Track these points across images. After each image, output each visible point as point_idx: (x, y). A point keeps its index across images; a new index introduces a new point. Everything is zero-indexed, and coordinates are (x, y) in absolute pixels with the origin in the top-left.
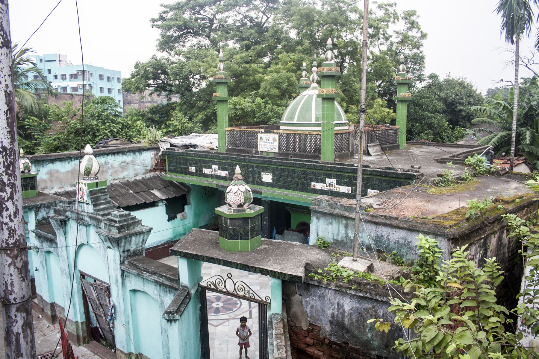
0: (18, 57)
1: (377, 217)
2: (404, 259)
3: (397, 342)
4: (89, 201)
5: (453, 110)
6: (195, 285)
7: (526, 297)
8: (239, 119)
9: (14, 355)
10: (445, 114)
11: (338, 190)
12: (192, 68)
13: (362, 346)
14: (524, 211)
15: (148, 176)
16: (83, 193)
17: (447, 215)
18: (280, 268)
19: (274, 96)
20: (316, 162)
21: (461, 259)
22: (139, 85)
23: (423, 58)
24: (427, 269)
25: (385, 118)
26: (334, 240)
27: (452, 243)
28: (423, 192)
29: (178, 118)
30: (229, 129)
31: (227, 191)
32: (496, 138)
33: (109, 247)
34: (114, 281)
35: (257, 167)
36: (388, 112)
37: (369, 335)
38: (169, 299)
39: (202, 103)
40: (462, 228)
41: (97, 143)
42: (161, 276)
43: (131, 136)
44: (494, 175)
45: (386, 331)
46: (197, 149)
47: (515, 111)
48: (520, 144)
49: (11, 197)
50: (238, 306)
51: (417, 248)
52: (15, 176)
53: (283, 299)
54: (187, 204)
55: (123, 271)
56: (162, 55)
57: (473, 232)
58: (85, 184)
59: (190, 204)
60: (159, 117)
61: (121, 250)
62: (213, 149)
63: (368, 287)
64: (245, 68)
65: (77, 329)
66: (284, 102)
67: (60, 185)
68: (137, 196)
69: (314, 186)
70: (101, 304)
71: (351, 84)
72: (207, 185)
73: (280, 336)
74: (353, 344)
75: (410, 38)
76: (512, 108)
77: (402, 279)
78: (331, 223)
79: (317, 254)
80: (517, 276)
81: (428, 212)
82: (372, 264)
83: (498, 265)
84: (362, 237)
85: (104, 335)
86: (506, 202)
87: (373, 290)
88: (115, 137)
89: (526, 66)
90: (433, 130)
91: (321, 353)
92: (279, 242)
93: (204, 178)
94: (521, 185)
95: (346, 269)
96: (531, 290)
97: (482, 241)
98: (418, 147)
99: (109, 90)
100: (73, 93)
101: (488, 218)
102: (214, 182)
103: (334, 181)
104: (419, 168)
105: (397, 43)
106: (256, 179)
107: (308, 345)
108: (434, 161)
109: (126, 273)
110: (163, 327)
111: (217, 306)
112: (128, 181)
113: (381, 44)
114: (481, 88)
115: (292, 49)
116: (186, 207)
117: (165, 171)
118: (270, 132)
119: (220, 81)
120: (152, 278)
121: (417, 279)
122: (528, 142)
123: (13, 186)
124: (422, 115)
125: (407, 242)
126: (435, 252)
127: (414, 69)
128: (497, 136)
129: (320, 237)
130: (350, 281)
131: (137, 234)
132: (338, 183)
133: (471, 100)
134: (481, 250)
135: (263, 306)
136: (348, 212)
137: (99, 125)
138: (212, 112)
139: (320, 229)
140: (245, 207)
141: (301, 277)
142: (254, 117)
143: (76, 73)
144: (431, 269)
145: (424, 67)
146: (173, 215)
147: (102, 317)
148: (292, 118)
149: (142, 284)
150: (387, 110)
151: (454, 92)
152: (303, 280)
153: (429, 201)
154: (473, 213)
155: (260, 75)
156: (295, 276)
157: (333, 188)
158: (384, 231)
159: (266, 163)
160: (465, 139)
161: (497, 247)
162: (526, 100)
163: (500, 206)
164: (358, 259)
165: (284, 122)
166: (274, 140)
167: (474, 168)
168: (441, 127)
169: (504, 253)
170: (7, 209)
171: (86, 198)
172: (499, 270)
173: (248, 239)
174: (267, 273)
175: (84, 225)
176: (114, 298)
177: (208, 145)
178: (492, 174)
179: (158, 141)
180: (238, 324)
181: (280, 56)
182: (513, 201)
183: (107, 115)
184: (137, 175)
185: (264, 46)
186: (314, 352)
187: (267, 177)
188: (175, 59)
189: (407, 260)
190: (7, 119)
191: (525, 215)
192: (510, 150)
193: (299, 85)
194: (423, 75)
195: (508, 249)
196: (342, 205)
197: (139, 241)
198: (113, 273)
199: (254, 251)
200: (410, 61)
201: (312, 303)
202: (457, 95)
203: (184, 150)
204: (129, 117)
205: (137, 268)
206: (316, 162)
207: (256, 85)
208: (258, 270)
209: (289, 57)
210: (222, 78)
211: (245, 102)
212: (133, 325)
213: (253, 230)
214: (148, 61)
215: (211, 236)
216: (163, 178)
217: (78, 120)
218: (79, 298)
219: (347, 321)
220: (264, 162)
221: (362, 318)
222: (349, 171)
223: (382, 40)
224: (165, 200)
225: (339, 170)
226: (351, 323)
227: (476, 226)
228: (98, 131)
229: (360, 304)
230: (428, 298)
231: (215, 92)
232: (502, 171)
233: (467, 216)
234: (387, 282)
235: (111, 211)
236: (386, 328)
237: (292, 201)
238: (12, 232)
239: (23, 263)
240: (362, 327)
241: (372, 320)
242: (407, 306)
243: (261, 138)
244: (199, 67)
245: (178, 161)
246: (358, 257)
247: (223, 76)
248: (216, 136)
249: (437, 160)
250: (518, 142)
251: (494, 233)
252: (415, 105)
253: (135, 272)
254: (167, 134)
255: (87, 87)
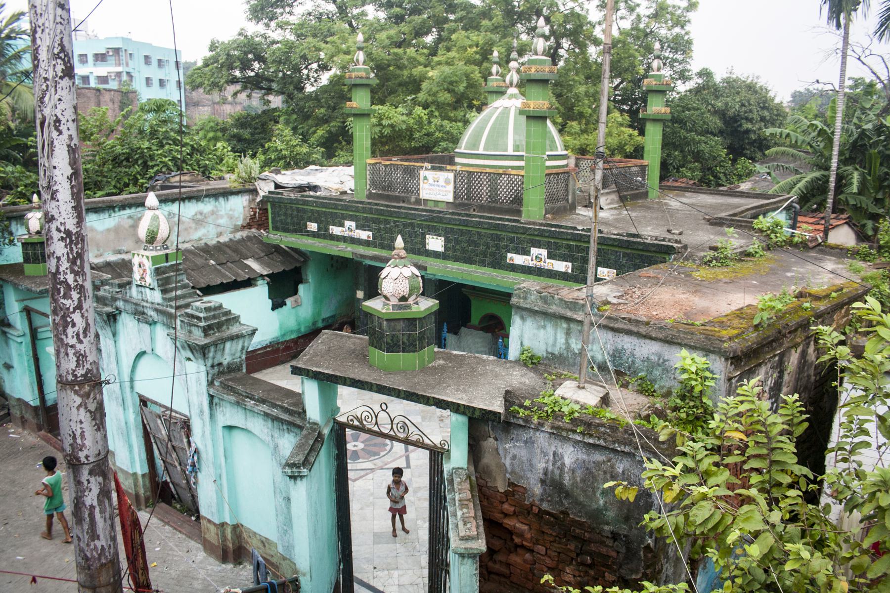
0: (7, 26)
1: (617, 320)
2: (656, 386)
3: (646, 517)
4: (155, 284)
5: (736, 130)
6: (328, 421)
7: (839, 453)
8: (389, 143)
9: (87, 537)
10: (722, 137)
11: (550, 268)
12: (306, 51)
13: (590, 518)
14: (843, 311)
15: (239, 235)
16: (144, 271)
17: (725, 319)
18: (465, 398)
19: (444, 104)
20: (515, 221)
21: (749, 399)
22: (217, 80)
23: (689, 42)
24: (692, 404)
25: (625, 144)
26: (548, 352)
27: (732, 364)
28: (686, 276)
29: (283, 137)
30: (373, 161)
31: (383, 276)
32: (804, 181)
33: (189, 359)
34: (198, 411)
35: (420, 226)
36: (630, 135)
37: (601, 502)
38: (287, 443)
39: (323, 110)
40: (747, 341)
41: (151, 178)
42: (274, 406)
43: (206, 166)
44: (799, 249)
45: (632, 499)
46: (318, 194)
47: (837, 139)
48: (842, 192)
49: (79, 307)
50: (388, 448)
51: (678, 371)
52: (84, 274)
53: (469, 444)
54: (301, 282)
55: (211, 397)
56: (255, 29)
57: (763, 346)
58: (148, 257)
59: (307, 282)
60: (250, 135)
61: (209, 363)
62: (344, 193)
63: (602, 429)
64: (396, 54)
65: (136, 485)
66: (460, 114)
67: (96, 252)
68: (223, 270)
69: (511, 259)
70: (173, 447)
71: (571, 85)
72: (337, 254)
73: (466, 503)
74: (575, 514)
75: (670, 9)
76: (833, 133)
77: (655, 419)
78: (544, 327)
79: (522, 376)
80: (827, 410)
81: (695, 311)
82: (608, 394)
83: (801, 406)
84: (592, 350)
85: (177, 494)
86: (817, 298)
87: (609, 435)
88: (179, 168)
89: (859, 59)
90: (701, 163)
91: (526, 528)
92: (462, 356)
93: (332, 242)
94: (840, 266)
95: (567, 401)
96: (847, 443)
97: (777, 358)
98: (677, 195)
99: (162, 83)
100: (101, 86)
101: (787, 325)
102: (349, 249)
103: (544, 252)
104: (681, 234)
105: (648, 16)
106: (417, 246)
107: (506, 515)
108: (703, 222)
109: (216, 400)
110: (277, 486)
111: (355, 449)
112: (206, 244)
113: (621, 18)
114: (782, 95)
115: (474, 24)
116: (301, 287)
117: (266, 228)
118: (441, 169)
119: (359, 81)
120: (260, 408)
121: (677, 419)
122: (855, 190)
123: (81, 289)
124: (685, 138)
125: (661, 361)
126: (706, 378)
127: (676, 61)
128: (806, 179)
129: (525, 348)
130: (573, 420)
131: (232, 338)
132: (550, 256)
133: (766, 113)
134: (774, 372)
135: (437, 455)
136: (571, 310)
137: (154, 148)
138: (339, 127)
139: (524, 335)
140: (411, 301)
141: (500, 413)
142: (411, 139)
143: (103, 52)
144: (698, 403)
145: (690, 57)
146: (280, 301)
147: (176, 467)
148: (475, 145)
149: (244, 417)
150: (631, 131)
151: (738, 100)
152: (502, 417)
153: (696, 292)
154: (765, 318)
155: (420, 68)
156: (491, 412)
157: (542, 263)
158: (627, 343)
159: (435, 219)
160: (753, 178)
161: (799, 368)
162: (855, 120)
163: (807, 305)
164: (586, 385)
165: (462, 150)
166: (447, 182)
167: (768, 235)
168: (715, 158)
169: (809, 376)
170: (74, 325)
171: (149, 280)
172: (801, 412)
173: (415, 351)
174: (446, 406)
175: (147, 322)
176: (197, 439)
177: (336, 186)
178: (796, 246)
179: (255, 179)
180: (389, 478)
181: (453, 37)
182: (828, 296)
183: (166, 131)
184: (220, 234)
185: (425, 16)
186: (514, 526)
187: (435, 243)
188: (276, 35)
189: (661, 387)
190: (72, 188)
191: (844, 317)
192: (825, 200)
193: (487, 88)
194: (689, 71)
195: (815, 369)
196: (561, 300)
197: (236, 350)
198: (195, 400)
199: (424, 369)
200: (669, 46)
201: (514, 451)
202: (743, 105)
203: (299, 195)
204: (201, 133)
205: (234, 392)
206: (515, 221)
207: (415, 85)
208: (431, 401)
209: (468, 38)
210: (362, 78)
211: (396, 115)
212: (228, 480)
213: (422, 337)
214: (231, 39)
215: (354, 344)
216: (265, 240)
217: (118, 139)
218: (137, 437)
219: (567, 480)
220: (432, 219)
221: (590, 476)
222: (569, 237)
223: (623, 12)
224: (267, 275)
225: (552, 235)
226: (574, 484)
227: (769, 337)
228: (152, 158)
229: (588, 455)
230: (699, 457)
231: (350, 100)
232: (811, 241)
233: (756, 322)
234: (631, 422)
235: (190, 300)
236: (631, 496)
237: (475, 282)
238: (81, 358)
239: (98, 403)
240: (590, 490)
241: (611, 484)
242: (670, 472)
243: (425, 178)
244: (320, 50)
245: (289, 212)
246: (586, 382)
247: (364, 74)
248: (351, 170)
249: (708, 220)
250: (839, 188)
251: (796, 346)
252: (677, 124)
253: (232, 398)
254: (266, 164)
255: (125, 77)
